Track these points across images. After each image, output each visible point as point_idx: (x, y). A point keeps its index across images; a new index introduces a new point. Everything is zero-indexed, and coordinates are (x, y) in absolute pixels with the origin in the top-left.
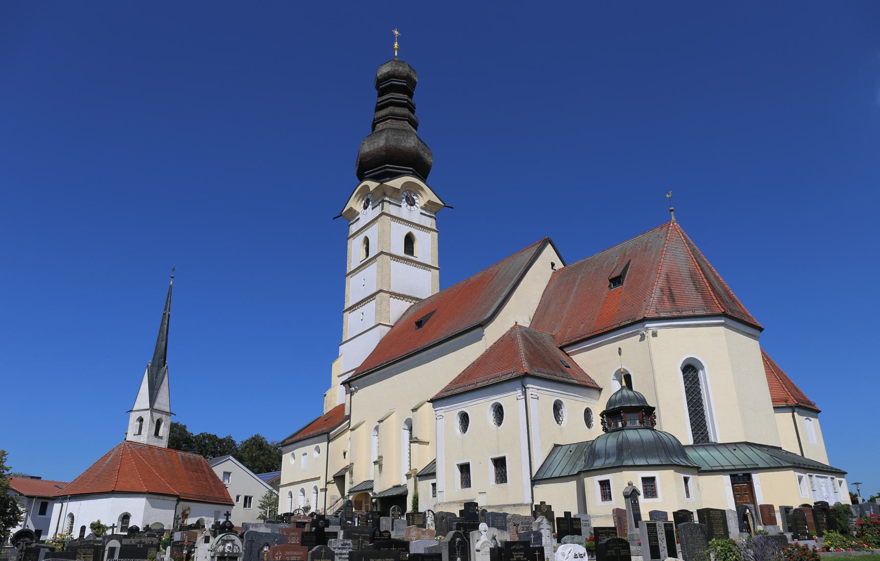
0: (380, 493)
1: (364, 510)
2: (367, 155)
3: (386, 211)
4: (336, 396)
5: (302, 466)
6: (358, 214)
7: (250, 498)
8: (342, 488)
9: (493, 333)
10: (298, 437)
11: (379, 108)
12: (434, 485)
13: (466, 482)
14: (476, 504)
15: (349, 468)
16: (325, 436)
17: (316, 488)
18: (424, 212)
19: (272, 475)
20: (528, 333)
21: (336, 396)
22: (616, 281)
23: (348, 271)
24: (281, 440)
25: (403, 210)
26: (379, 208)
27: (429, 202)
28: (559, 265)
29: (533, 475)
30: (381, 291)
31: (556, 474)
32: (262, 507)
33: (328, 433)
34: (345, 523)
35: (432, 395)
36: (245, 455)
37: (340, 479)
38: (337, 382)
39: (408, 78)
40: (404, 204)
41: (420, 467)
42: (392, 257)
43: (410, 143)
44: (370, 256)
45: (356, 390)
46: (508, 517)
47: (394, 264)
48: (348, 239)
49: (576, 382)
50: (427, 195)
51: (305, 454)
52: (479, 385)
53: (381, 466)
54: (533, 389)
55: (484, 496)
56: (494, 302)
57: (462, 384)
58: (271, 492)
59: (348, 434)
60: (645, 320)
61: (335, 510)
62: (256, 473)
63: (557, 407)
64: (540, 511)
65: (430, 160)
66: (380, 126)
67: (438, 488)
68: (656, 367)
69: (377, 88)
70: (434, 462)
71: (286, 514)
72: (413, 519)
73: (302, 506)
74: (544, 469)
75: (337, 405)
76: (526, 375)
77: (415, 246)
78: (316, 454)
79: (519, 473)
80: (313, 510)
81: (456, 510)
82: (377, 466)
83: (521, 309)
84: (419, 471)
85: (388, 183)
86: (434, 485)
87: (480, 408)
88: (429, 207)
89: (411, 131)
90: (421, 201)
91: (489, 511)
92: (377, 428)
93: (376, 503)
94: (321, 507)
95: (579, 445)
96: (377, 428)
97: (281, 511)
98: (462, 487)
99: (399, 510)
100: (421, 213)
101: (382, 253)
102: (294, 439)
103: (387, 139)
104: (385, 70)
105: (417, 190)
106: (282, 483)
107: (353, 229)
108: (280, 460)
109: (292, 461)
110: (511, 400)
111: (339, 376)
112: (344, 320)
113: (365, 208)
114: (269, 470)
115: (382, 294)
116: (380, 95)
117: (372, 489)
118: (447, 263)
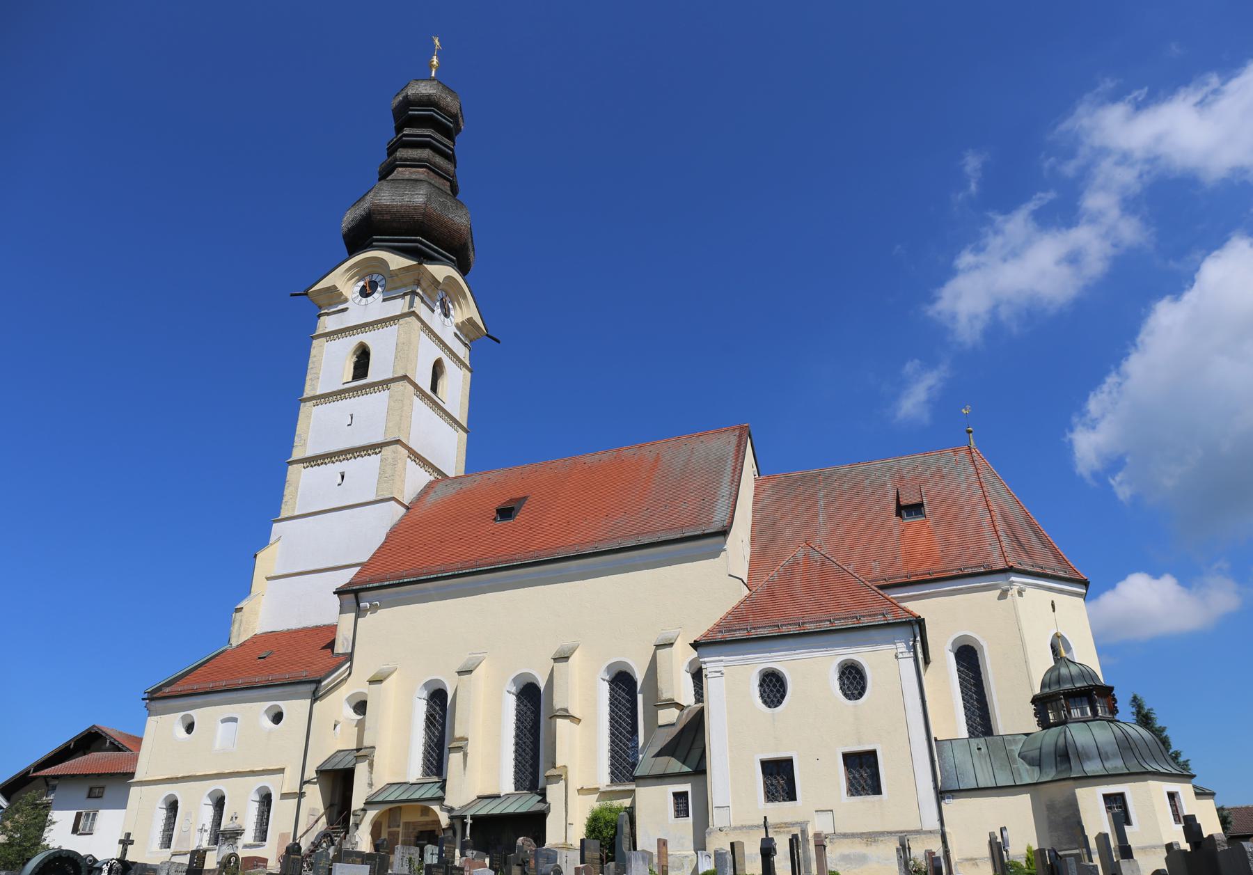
2: (387, 210)
5: (218, 746)
6: (346, 300)
10: (177, 688)
22: (506, 513)
25: (435, 319)
27: (470, 320)
33: (319, 682)
40: (438, 311)
43: (459, 219)
45: (374, 609)
50: (467, 311)
60: (1010, 570)
68: (1027, 638)
75: (258, 631)
104: (424, 89)
107: (328, 323)
113: (364, 293)
115: (399, 447)
118: (480, 428)
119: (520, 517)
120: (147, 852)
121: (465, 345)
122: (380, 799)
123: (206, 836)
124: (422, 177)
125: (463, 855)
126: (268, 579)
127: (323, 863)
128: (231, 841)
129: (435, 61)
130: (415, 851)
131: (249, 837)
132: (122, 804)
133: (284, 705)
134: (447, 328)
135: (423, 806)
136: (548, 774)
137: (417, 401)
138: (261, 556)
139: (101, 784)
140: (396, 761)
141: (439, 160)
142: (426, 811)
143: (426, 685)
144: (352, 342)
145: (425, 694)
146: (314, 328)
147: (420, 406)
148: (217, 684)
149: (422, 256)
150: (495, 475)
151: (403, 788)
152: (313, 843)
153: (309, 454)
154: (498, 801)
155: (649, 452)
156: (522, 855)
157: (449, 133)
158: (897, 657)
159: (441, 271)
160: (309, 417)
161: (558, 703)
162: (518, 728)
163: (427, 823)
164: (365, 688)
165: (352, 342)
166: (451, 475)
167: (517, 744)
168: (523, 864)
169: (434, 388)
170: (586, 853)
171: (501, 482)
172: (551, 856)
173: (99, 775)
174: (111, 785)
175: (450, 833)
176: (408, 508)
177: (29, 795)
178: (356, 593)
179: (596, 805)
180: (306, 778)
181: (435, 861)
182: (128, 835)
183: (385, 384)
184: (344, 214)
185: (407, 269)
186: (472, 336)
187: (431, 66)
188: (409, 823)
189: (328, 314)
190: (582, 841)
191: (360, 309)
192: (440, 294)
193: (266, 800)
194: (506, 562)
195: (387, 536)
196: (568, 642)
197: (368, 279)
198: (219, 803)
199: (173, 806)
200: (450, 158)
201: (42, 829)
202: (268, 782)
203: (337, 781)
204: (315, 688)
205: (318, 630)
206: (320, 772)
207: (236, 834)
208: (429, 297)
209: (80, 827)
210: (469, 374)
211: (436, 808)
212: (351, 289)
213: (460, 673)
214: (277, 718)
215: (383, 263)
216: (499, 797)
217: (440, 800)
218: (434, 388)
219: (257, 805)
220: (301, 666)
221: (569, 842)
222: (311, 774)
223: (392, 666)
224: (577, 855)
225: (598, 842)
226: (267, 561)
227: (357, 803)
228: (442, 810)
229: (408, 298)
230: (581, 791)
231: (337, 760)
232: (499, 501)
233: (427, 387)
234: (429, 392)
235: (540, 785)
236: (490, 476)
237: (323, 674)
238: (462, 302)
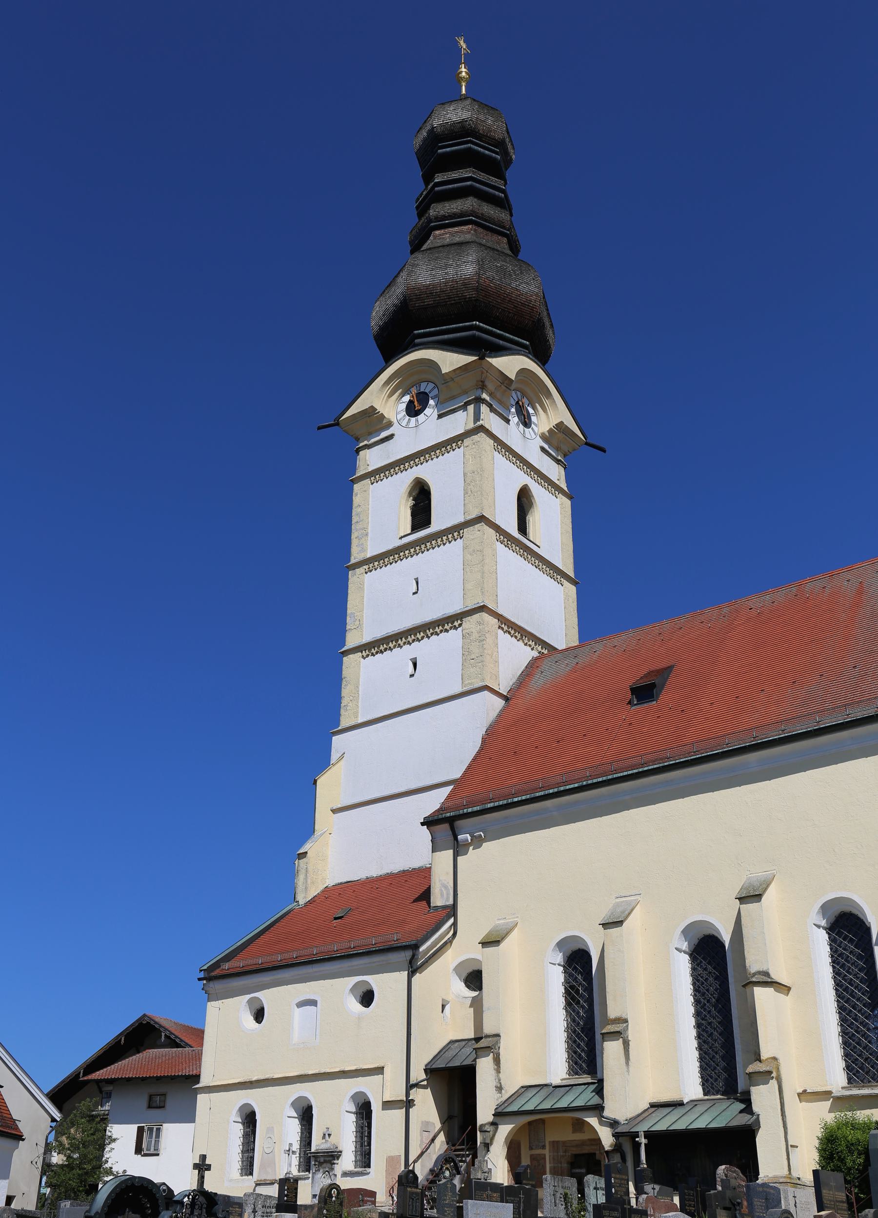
2: (428, 291)
5: (296, 1036)
6: (390, 424)
18: (546, 447)
22: (644, 692)
25: (511, 432)
27: (560, 426)
33: (415, 947)
40: (514, 420)
43: (527, 286)
45: (477, 842)
48: (354, 482)
50: (554, 414)
75: (331, 882)
88: (556, 438)
104: (454, 114)
107: (372, 459)
113: (413, 411)
115: (485, 615)
118: (594, 576)
119: (666, 697)
120: (226, 1181)
121: (558, 462)
122: (514, 1108)
123: (295, 1160)
124: (468, 237)
125: (640, 1191)
126: (334, 811)
127: (448, 1199)
128: (327, 1167)
129: (464, 71)
130: (571, 1184)
131: (347, 1161)
132: (189, 1116)
133: (375, 981)
134: (529, 443)
135: (574, 1118)
136: (751, 1069)
137: (500, 547)
138: (323, 781)
139: (161, 1090)
140: (531, 1054)
141: (488, 210)
142: (580, 1125)
143: (560, 945)
144: (403, 480)
145: (559, 958)
146: (354, 468)
147: (508, 559)
148: (286, 956)
149: (482, 348)
150: (624, 640)
151: (544, 1092)
152: (432, 1171)
153: (367, 638)
154: (679, 1111)
155: (846, 581)
156: (729, 1194)
157: (497, 169)
159: (511, 364)
160: (361, 588)
161: (754, 963)
162: (697, 1002)
163: (583, 1143)
164: (477, 953)
165: (403, 480)
166: (561, 645)
167: (698, 1026)
168: (732, 1207)
169: (523, 528)
170: (825, 1192)
171: (633, 649)
172: (771, 1195)
173: (158, 1079)
174: (171, 1092)
175: (617, 1158)
176: (506, 699)
177: (84, 1105)
178: (451, 821)
179: (831, 1118)
180: (413, 1080)
181: (602, 1199)
182: (203, 1157)
183: (455, 531)
184: (372, 308)
185: (465, 368)
186: (565, 448)
187: (459, 80)
188: (557, 1141)
190: (815, 1173)
191: (411, 434)
192: (515, 396)
193: (364, 1111)
194: (654, 762)
195: (484, 740)
196: (754, 872)
197: (414, 391)
198: (306, 1115)
199: (249, 1119)
200: (503, 203)
201: (102, 1148)
202: (369, 1086)
203: (454, 1082)
204: (412, 957)
205: (405, 875)
206: (430, 1071)
207: (330, 1157)
208: (501, 402)
209: (144, 1146)
210: (568, 503)
211: (593, 1121)
212: (393, 408)
213: (606, 925)
214: (367, 998)
215: (432, 365)
216: (679, 1104)
217: (598, 1109)
218: (523, 528)
219: (353, 1117)
220: (389, 927)
221: (795, 1174)
222: (418, 1074)
223: (510, 920)
224: (809, 1195)
225: (840, 1176)
226: (330, 789)
227: (484, 1114)
228: (601, 1123)
229: (471, 408)
230: (804, 1096)
231: (450, 1054)
232: (634, 676)
233: (511, 526)
234: (515, 533)
235: (741, 1086)
236: (615, 642)
237: (420, 936)
238: (546, 402)
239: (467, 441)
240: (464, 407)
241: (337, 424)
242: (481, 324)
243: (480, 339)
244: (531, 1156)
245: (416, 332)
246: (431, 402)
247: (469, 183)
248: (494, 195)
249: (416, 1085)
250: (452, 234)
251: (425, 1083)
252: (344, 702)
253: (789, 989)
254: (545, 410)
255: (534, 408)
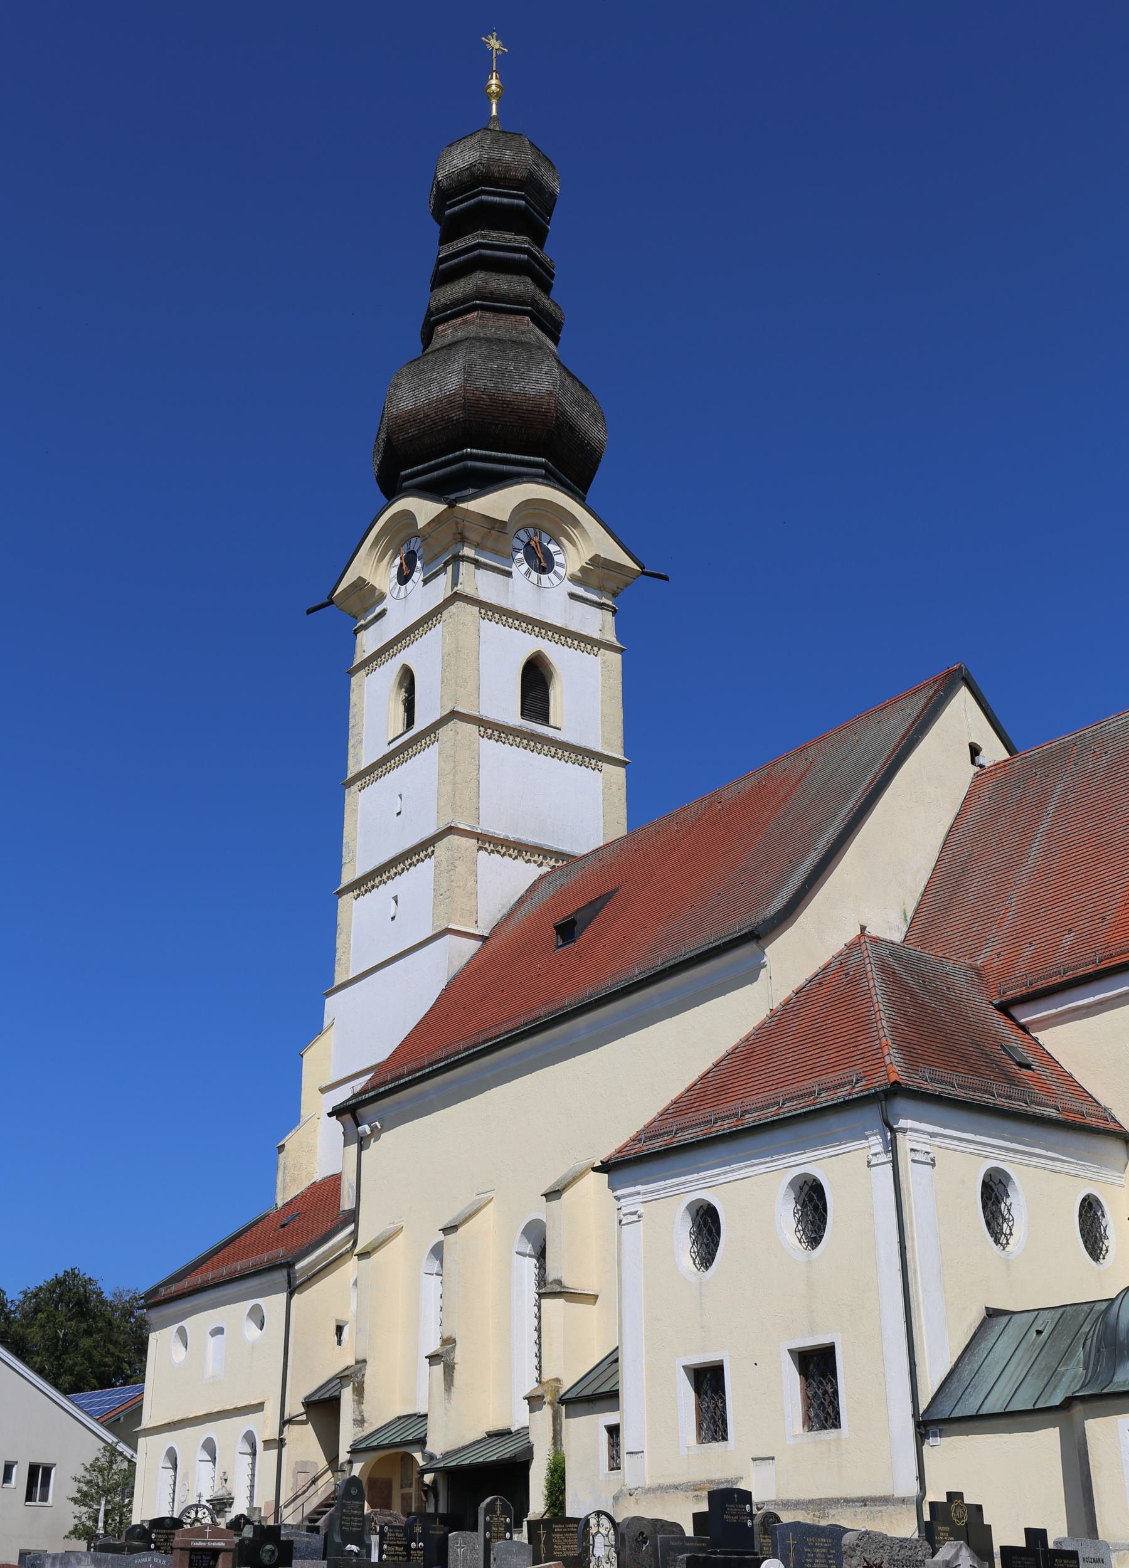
0: (446, 1455)
1: (396, 1509)
3: (464, 587)
4: (315, 1149)
6: (382, 597)
7: (47, 1471)
8: (329, 1439)
9: (794, 959)
10: (197, 1279)
11: (442, 278)
12: (614, 1431)
13: (713, 1423)
14: (746, 1496)
15: (352, 1376)
16: (281, 1276)
17: (249, 1437)
18: (580, 591)
19: (113, 1397)
20: (898, 959)
21: (315, 1149)
23: (353, 770)
24: (144, 1288)
25: (519, 588)
26: (444, 580)
27: (596, 560)
28: (994, 752)
29: (923, 1406)
30: (451, 830)
31: (994, 1405)
32: (83, 1499)
33: (290, 1265)
34: (340, 1550)
35: (606, 1150)
36: (34, 1335)
37: (323, 1409)
38: (316, 1105)
39: (531, 185)
40: (520, 568)
41: (568, 1373)
42: (483, 721)
43: (538, 382)
44: (420, 725)
45: (376, 1133)
46: (847, 1539)
47: (490, 748)
48: (352, 673)
49: (1051, 1113)
50: (589, 542)
51: (218, 1331)
52: (750, 1119)
53: (449, 1370)
54: (917, 1132)
55: (766, 1468)
56: (795, 865)
57: (699, 1116)
58: (112, 1451)
59: (352, 1266)
61: (309, 1508)
62: (65, 1392)
63: (994, 1191)
64: (949, 1522)
65: (596, 433)
66: (446, 333)
67: (628, 1441)
69: (438, 214)
70: (613, 1360)
71: (158, 1523)
72: (549, 1542)
73: (207, 1495)
74: (956, 1389)
75: (318, 1177)
76: (896, 1091)
77: (552, 693)
78: (251, 1331)
79: (878, 1398)
80: (240, 1508)
81: (682, 1513)
82: (439, 1369)
83: (877, 885)
84: (566, 1385)
85: (473, 506)
86: (614, 1431)
87: (753, 1193)
88: (596, 576)
89: (541, 347)
90: (571, 558)
91: (786, 1517)
92: (437, 1251)
93: (433, 1488)
94: (264, 1498)
95: (1067, 1313)
96: (437, 1251)
97: (142, 1511)
98: (702, 1438)
99: (505, 1512)
100: (573, 596)
101: (454, 715)
102: (185, 1284)
103: (468, 372)
104: (461, 158)
105: (558, 524)
106: (147, 1421)
107: (368, 642)
108: (142, 1349)
109: (179, 1354)
110: (849, 1167)
111: (323, 1090)
112: (341, 918)
113: (403, 578)
114: (105, 1382)
115: (453, 839)
116: (445, 239)
117: (421, 1442)
119: (585, 937)
121: (601, 606)
153: (359, 874)
158: (869, 1165)
186: (612, 586)
189: (365, 627)
210: (617, 658)
222: (295, 1407)
229: (450, 569)
238: (574, 533)
239: (446, 614)
240: (443, 570)
241: (331, 602)
242: (474, 451)
243: (474, 470)
244: (402, 1495)
245: (403, 473)
246: (419, 564)
247: (476, 252)
248: (513, 260)
249: (290, 1421)
250: (455, 330)
251: (304, 1417)
252: (338, 954)
253: (596, 1297)
254: (573, 543)
255: (559, 544)
